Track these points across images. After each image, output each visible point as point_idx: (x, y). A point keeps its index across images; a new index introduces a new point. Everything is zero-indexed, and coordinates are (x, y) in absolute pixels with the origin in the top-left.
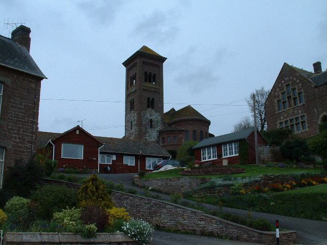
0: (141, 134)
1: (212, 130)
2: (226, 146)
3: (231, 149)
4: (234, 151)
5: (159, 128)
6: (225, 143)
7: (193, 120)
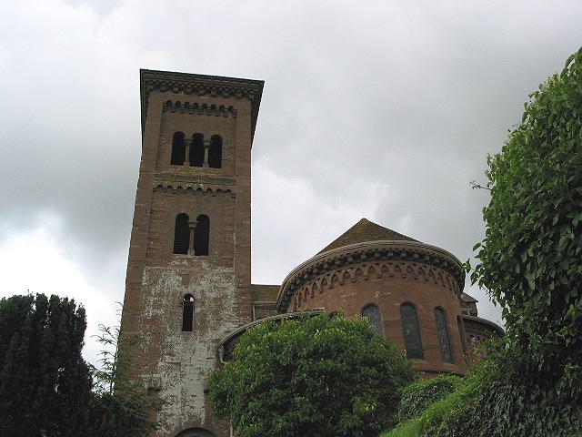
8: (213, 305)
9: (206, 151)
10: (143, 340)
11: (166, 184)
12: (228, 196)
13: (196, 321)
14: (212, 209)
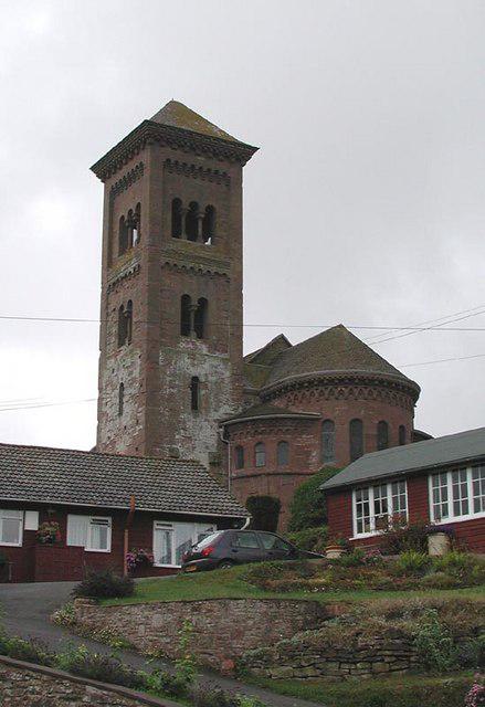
0: (157, 433)
1: (426, 418)
2: (444, 482)
3: (460, 492)
4: (471, 497)
5: (226, 410)
6: (440, 470)
7: (349, 381)
9: (200, 224)
11: (189, 265)
12: (223, 280)
13: (202, 403)
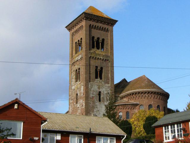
8: (106, 95)
9: (100, 44)
10: (90, 103)
14: (104, 64)
